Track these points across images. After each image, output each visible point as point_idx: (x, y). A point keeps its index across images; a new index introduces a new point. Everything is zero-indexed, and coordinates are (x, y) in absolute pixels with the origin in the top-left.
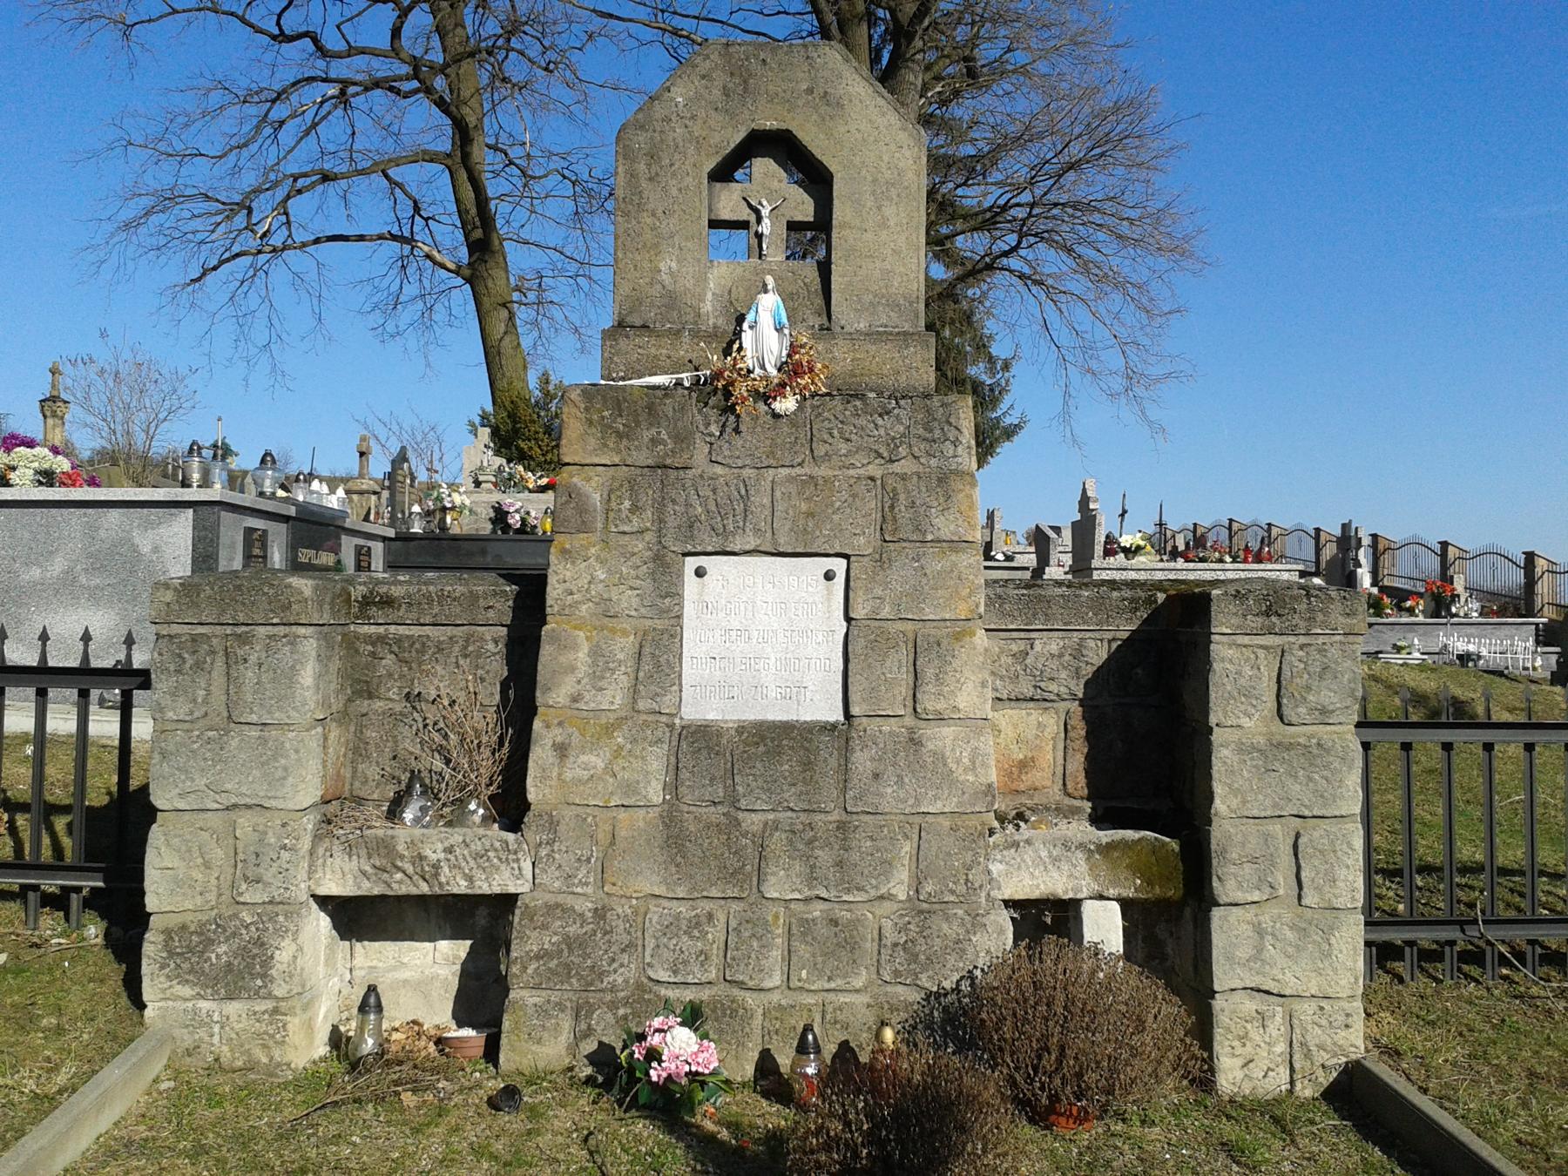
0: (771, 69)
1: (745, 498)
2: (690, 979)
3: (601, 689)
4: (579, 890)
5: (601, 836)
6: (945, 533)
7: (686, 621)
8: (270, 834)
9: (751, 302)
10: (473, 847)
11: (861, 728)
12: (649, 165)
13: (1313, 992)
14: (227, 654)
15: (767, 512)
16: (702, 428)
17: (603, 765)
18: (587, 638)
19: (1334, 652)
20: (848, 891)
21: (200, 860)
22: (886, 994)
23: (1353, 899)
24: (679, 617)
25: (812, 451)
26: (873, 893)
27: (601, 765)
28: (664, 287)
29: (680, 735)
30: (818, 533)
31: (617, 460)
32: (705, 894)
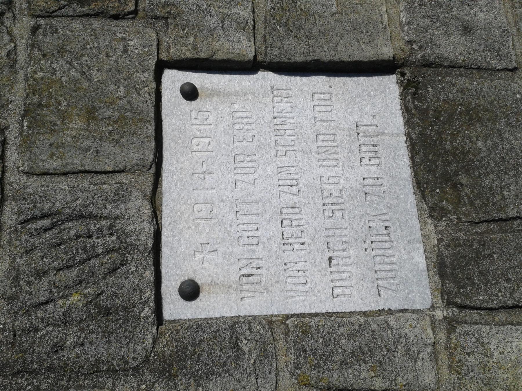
7: (273, 310)
11: (407, 48)
15: (85, 182)
29: (461, 307)
30: (121, 103)
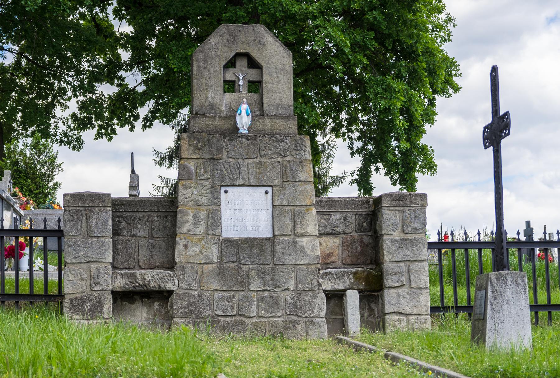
0: (242, 33)
1: (239, 168)
2: (228, 314)
3: (197, 228)
4: (193, 288)
5: (199, 272)
6: (302, 179)
8: (101, 269)
9: (238, 107)
10: (160, 276)
12: (204, 64)
13: (415, 313)
14: (86, 215)
16: (225, 146)
17: (199, 251)
18: (192, 212)
19: (418, 212)
20: (276, 288)
21: (80, 278)
22: (288, 318)
23: (426, 285)
24: (220, 205)
25: (260, 153)
26: (283, 288)
27: (198, 250)
28: (210, 102)
31: (199, 157)
32: (232, 289)
